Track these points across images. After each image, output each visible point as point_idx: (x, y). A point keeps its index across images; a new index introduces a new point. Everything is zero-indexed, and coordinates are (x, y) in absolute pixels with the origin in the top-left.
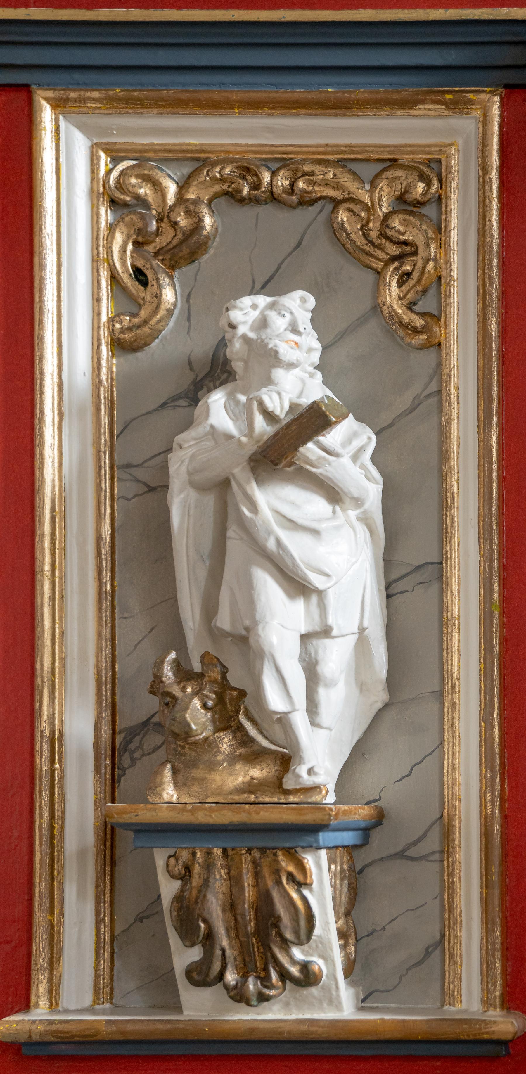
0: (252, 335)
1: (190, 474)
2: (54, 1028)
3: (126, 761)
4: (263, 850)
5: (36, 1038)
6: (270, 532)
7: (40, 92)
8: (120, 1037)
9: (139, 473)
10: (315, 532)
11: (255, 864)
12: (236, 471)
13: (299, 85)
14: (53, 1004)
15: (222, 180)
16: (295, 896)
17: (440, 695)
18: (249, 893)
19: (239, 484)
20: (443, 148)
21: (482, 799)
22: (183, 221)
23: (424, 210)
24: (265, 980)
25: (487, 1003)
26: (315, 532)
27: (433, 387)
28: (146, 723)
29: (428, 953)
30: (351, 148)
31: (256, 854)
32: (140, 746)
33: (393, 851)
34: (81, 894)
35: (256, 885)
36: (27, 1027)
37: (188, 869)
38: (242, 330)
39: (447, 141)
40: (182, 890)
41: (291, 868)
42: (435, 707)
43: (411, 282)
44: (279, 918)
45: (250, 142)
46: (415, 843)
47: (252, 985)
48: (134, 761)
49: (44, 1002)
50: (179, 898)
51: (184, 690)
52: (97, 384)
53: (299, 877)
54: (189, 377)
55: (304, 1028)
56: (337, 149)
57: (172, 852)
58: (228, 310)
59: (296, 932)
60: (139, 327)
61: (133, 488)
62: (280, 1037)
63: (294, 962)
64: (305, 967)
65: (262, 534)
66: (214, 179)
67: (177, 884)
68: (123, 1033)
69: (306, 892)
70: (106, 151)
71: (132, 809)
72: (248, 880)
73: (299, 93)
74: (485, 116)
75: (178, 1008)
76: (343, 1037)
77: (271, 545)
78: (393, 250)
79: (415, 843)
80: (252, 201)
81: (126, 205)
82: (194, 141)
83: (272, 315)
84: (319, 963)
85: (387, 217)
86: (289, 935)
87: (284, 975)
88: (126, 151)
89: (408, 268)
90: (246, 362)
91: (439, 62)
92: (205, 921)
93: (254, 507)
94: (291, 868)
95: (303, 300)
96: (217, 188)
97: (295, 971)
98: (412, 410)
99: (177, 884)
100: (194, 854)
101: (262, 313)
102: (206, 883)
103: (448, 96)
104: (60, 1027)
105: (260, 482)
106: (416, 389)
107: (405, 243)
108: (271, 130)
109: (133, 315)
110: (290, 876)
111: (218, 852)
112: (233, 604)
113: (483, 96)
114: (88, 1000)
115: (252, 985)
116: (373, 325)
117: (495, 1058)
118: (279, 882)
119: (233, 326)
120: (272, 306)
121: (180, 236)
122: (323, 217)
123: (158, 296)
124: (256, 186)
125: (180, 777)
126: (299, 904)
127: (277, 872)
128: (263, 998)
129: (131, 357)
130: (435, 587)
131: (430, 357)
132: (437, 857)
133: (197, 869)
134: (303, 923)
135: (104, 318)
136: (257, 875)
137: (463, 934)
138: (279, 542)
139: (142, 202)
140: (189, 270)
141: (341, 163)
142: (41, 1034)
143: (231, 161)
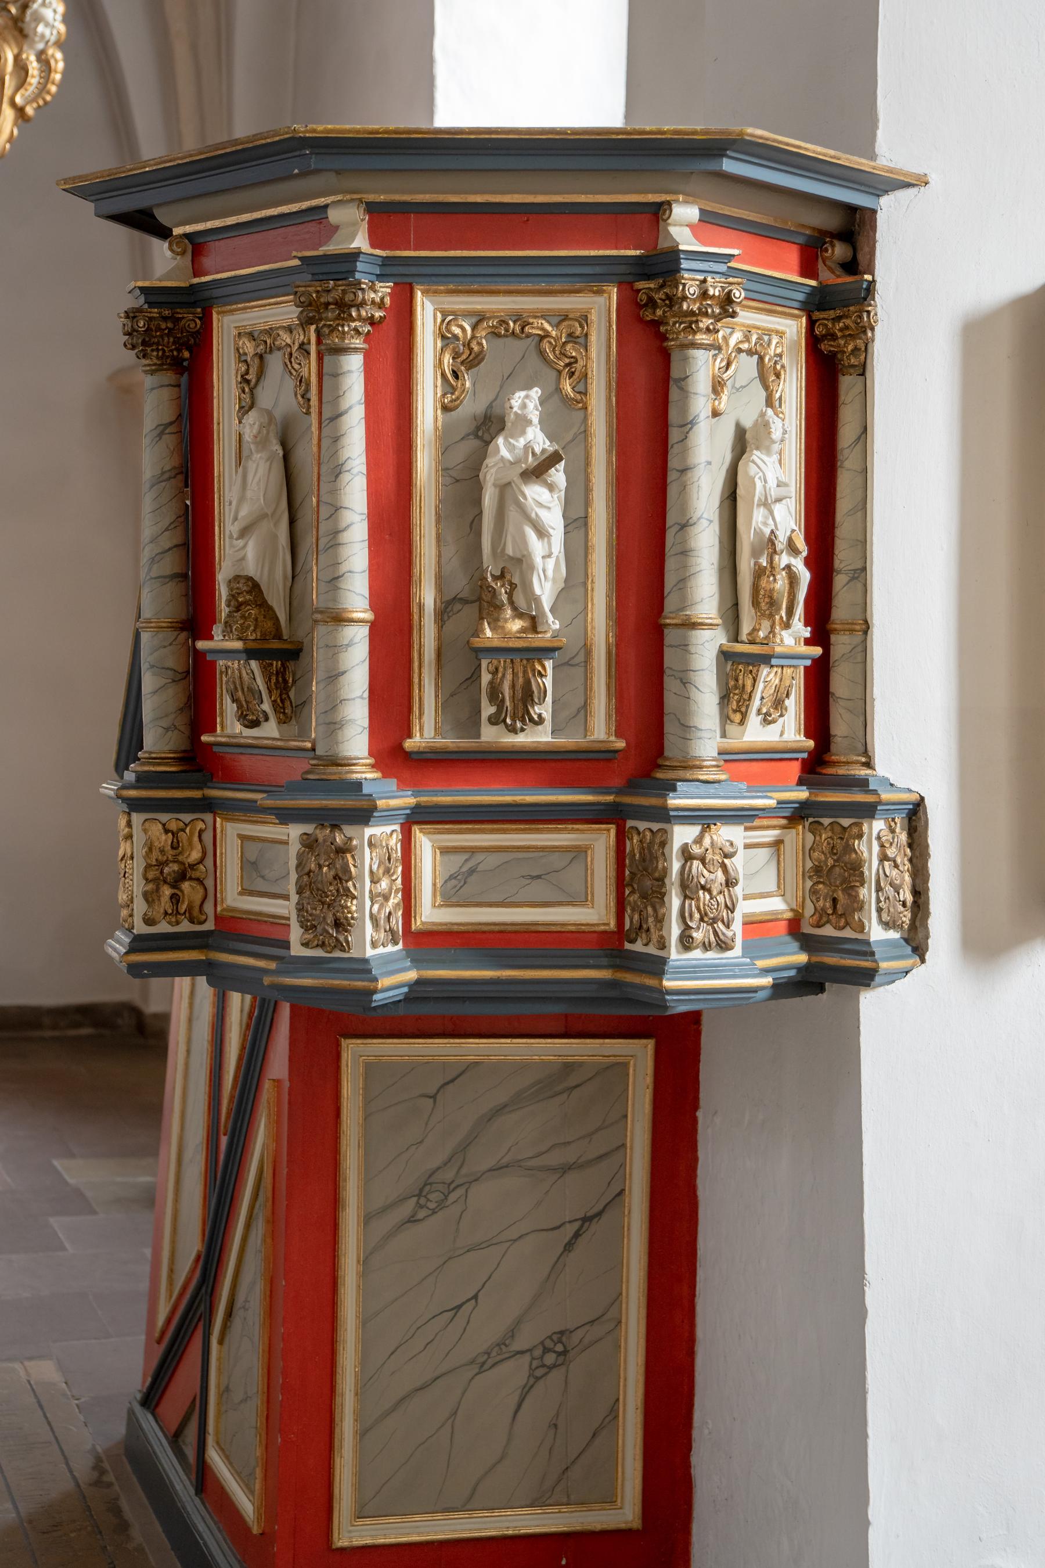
0: (519, 412)
1: (495, 480)
2: (429, 745)
3: (446, 618)
4: (528, 660)
5: (421, 749)
6: (532, 509)
7: (418, 287)
8: (457, 750)
9: (451, 472)
10: (549, 508)
11: (525, 667)
12: (515, 479)
13: (529, 282)
14: (422, 735)
15: (493, 326)
16: (539, 680)
17: (585, 584)
18: (521, 680)
19: (516, 485)
20: (590, 309)
21: (607, 636)
22: (476, 348)
23: (579, 340)
24: (523, 721)
25: (609, 734)
26: (549, 508)
27: (582, 429)
28: (454, 598)
29: (578, 711)
30: (549, 310)
31: (525, 662)
32: (452, 610)
33: (563, 662)
34: (430, 684)
35: (524, 676)
36: (418, 744)
37: (497, 669)
38: (515, 409)
39: (591, 306)
40: (493, 679)
41: (540, 668)
42: (582, 590)
43: (575, 377)
44: (533, 692)
45: (504, 307)
46: (573, 658)
47: (519, 725)
48: (449, 617)
49: (418, 735)
50: (491, 683)
51: (496, 584)
52: (436, 428)
53: (543, 673)
54: (475, 424)
55: (535, 745)
56: (542, 310)
57: (490, 660)
58: (509, 400)
59: (539, 699)
60: (455, 401)
61: (449, 480)
62: (524, 750)
63: (535, 713)
64: (540, 715)
65: (529, 510)
66: (489, 327)
67: (490, 676)
68: (459, 747)
69: (544, 680)
70: (440, 312)
71: (507, 642)
72: (521, 675)
73: (529, 286)
74: (610, 298)
75: (479, 736)
76: (552, 749)
77: (533, 515)
78: (567, 361)
79: (573, 658)
80: (505, 336)
81: (448, 338)
82: (479, 307)
83: (527, 401)
84: (545, 715)
85: (564, 343)
86: (536, 700)
87: (531, 720)
88: (449, 311)
89: (573, 370)
90: (512, 423)
91: (591, 272)
92: (502, 693)
93: (525, 498)
94: (540, 668)
95: (537, 392)
96: (490, 330)
97: (535, 717)
98: (573, 440)
99: (490, 676)
100: (500, 662)
101: (523, 400)
102: (504, 675)
103: (595, 288)
104: (432, 744)
105: (525, 483)
106: (574, 430)
107: (572, 357)
108: (514, 302)
109: (452, 394)
110: (539, 672)
111: (508, 661)
112: (514, 541)
113: (610, 288)
114: (432, 735)
115: (519, 725)
116: (556, 398)
117: (609, 760)
118: (534, 675)
119: (511, 408)
120: (527, 397)
121: (473, 355)
122: (534, 343)
123: (463, 385)
124: (507, 330)
125: (492, 626)
126: (541, 685)
127: (534, 670)
128: (522, 730)
129: (449, 414)
130: (583, 529)
131: (581, 413)
132: (583, 664)
133: (501, 670)
134: (542, 694)
135: (439, 395)
136: (525, 672)
137: (596, 701)
138: (537, 514)
139: (456, 337)
140: (474, 370)
141: (543, 317)
142: (424, 748)
143: (497, 317)
